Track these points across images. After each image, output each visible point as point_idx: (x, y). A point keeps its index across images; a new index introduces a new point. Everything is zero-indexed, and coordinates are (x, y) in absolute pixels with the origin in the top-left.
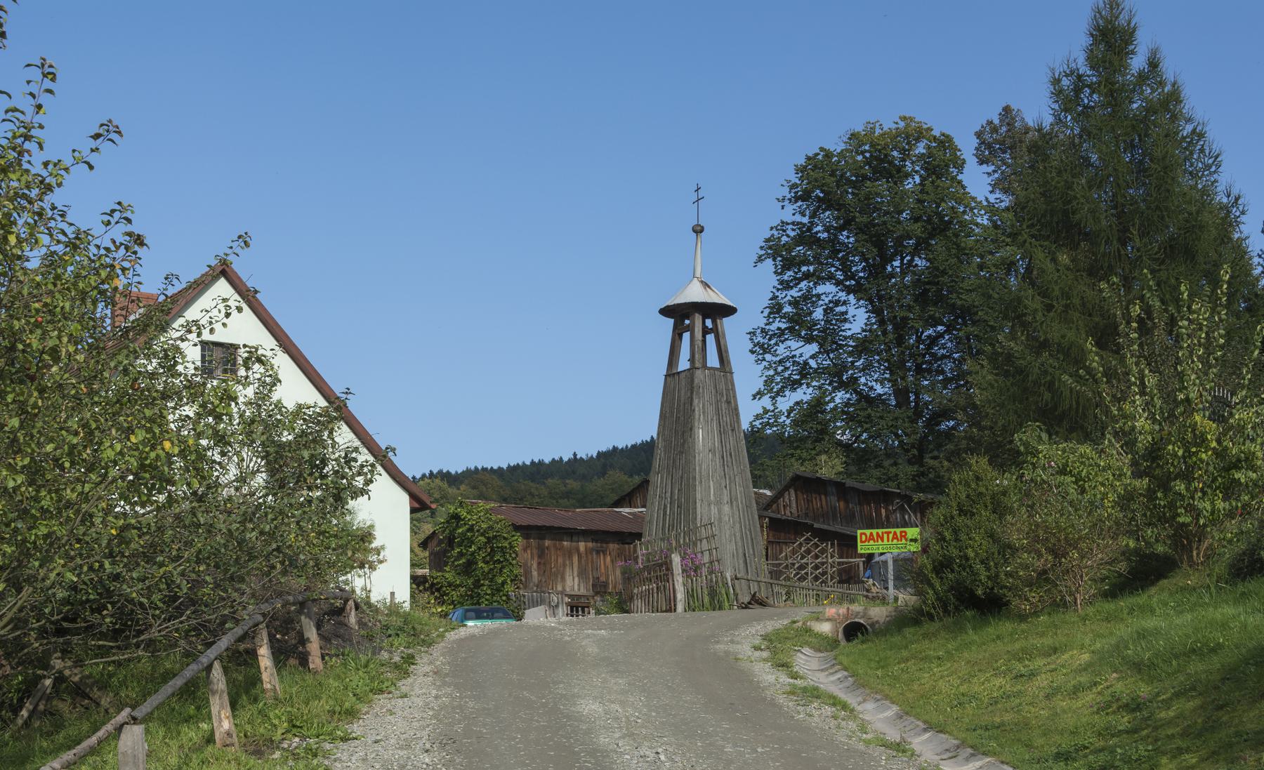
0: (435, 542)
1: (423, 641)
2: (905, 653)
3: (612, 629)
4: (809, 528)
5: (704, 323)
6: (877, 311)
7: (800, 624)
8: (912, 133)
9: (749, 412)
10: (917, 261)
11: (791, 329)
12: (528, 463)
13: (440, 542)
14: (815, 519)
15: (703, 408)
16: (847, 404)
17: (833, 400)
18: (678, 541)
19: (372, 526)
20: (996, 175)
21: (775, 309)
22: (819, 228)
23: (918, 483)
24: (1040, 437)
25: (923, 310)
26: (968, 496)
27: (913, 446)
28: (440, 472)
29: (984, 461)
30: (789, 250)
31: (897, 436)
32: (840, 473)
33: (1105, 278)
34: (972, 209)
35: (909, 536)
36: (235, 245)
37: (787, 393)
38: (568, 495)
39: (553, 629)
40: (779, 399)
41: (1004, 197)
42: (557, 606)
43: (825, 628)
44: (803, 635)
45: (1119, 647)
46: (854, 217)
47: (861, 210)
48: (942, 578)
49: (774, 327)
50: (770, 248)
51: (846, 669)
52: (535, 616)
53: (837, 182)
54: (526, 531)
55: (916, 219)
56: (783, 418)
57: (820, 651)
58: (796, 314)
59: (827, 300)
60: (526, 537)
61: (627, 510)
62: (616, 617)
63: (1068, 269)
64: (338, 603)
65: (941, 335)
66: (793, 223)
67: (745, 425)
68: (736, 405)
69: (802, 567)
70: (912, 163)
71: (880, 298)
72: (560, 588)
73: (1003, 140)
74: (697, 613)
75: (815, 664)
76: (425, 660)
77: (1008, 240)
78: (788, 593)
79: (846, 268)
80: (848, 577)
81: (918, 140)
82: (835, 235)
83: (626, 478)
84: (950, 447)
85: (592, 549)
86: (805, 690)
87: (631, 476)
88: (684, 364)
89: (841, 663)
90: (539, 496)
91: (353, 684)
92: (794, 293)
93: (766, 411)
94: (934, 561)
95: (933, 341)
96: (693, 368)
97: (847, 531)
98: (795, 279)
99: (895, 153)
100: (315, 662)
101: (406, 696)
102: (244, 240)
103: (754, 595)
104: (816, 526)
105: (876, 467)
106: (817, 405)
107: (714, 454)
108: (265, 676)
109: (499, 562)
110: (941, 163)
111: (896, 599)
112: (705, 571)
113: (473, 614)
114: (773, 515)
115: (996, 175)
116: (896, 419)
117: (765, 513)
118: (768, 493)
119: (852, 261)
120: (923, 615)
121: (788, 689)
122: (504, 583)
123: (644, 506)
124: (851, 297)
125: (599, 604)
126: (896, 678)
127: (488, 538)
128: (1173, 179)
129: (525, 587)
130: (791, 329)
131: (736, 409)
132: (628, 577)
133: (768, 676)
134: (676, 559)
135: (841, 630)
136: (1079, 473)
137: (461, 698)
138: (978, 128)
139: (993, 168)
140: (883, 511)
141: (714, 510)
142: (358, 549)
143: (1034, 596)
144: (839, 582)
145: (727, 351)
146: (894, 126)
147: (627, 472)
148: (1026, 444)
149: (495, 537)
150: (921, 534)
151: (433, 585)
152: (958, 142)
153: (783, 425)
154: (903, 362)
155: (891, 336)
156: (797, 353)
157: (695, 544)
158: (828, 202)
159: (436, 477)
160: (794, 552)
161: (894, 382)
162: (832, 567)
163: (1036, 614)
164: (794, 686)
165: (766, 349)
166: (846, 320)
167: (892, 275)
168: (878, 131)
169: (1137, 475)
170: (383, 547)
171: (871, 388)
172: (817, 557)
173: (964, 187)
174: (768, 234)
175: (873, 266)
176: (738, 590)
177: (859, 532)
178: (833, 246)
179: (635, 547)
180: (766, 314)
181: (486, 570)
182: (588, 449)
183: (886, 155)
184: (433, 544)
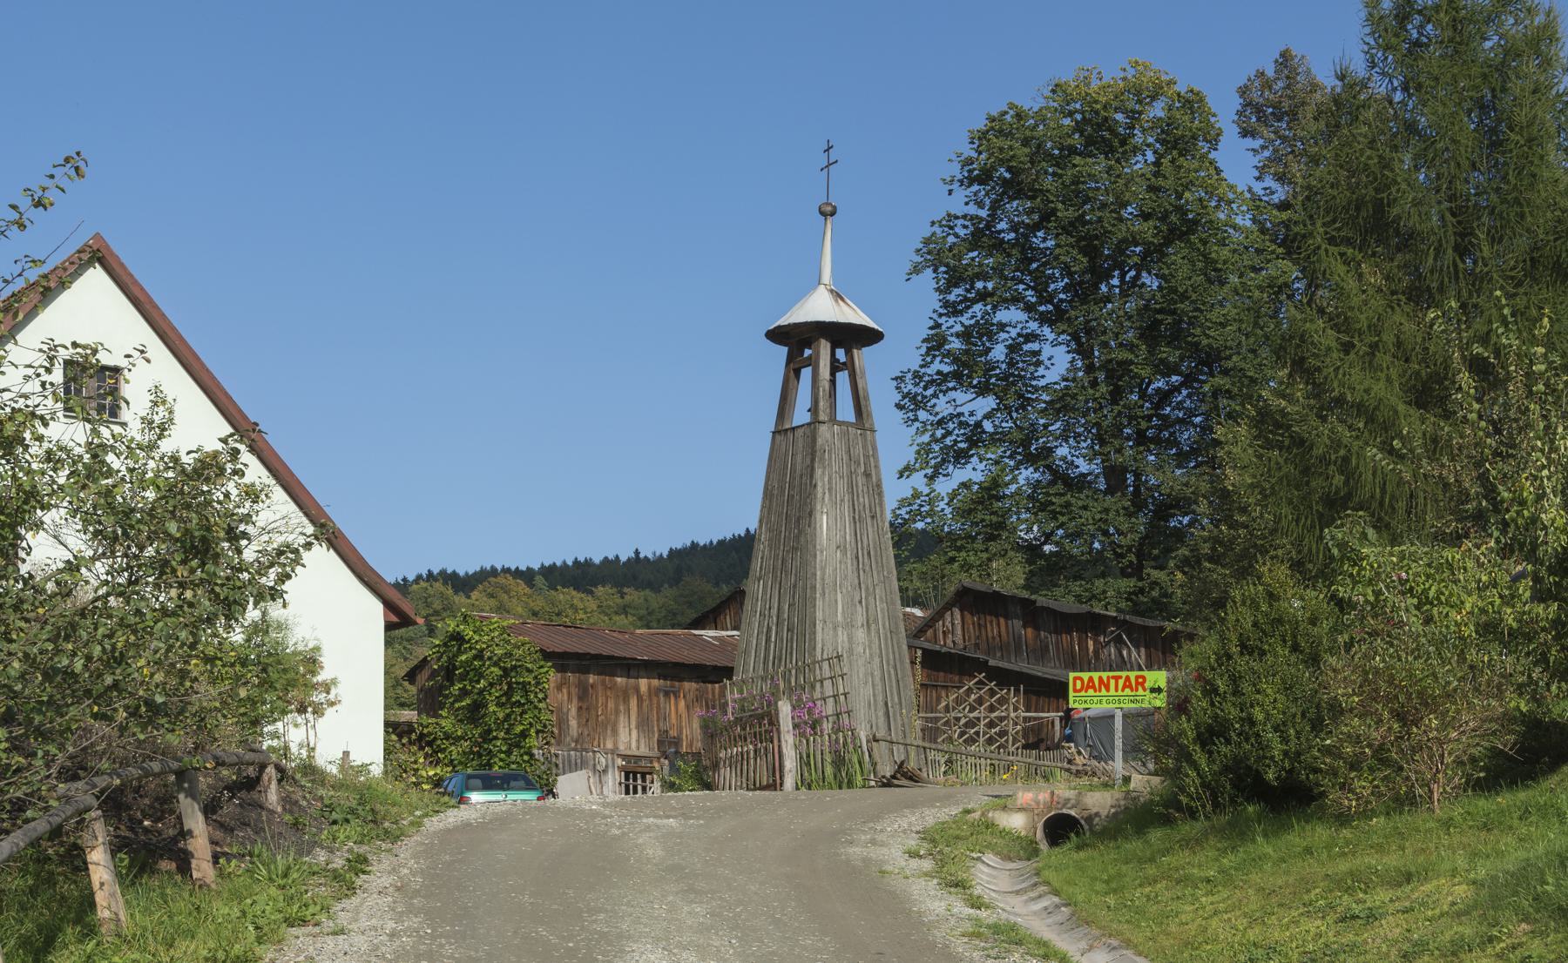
0: (425, 674)
1: (386, 832)
2: (1151, 871)
3: (686, 816)
4: (982, 666)
5: (833, 354)
6: (1083, 351)
7: (977, 815)
8: (1144, 92)
9: (895, 491)
10: (1146, 279)
11: (957, 376)
13: (434, 674)
14: (990, 651)
15: (829, 482)
16: (1037, 485)
19: (317, 649)
20: (1267, 154)
21: (936, 343)
22: (1003, 225)
23: (1135, 604)
24: (1364, 535)
25: (1151, 352)
26: (1255, 624)
27: (1129, 549)
28: (443, 573)
29: (1283, 571)
31: (1106, 533)
33: (1433, 303)
34: (1230, 203)
36: (58, 172)
41: (1274, 185)
42: (605, 771)
43: (1016, 822)
44: (982, 833)
45: (1523, 877)
47: (1062, 210)
48: (1210, 753)
50: (929, 253)
51: (1056, 893)
52: (573, 788)
54: (563, 661)
55: (1146, 217)
57: (1010, 859)
58: (966, 352)
59: (1014, 334)
60: (561, 669)
61: (712, 633)
62: (695, 797)
63: (1380, 290)
64: (251, 771)
65: (1176, 389)
66: (964, 217)
68: (879, 480)
69: (971, 724)
70: (1144, 131)
72: (609, 745)
73: (1274, 106)
74: (816, 793)
75: (1004, 882)
76: (386, 865)
77: (1281, 250)
78: (949, 762)
79: (1040, 287)
80: (1036, 740)
81: (1153, 98)
82: (1026, 236)
84: (1184, 552)
85: (658, 690)
86: (996, 929)
87: (717, 584)
88: (801, 416)
89: (1047, 883)
91: (258, 909)
92: (966, 319)
93: (916, 495)
94: (1197, 726)
95: (1165, 396)
96: (815, 422)
97: (1046, 671)
98: (966, 299)
99: (1119, 117)
100: (203, 868)
101: (342, 932)
102: (74, 165)
104: (992, 663)
106: (991, 491)
107: (844, 553)
108: (100, 898)
110: (1184, 137)
112: (827, 726)
113: (478, 782)
114: (927, 645)
115: (1267, 154)
116: (1107, 511)
117: (917, 643)
118: (918, 612)
121: (968, 927)
124: (1046, 330)
126: (1140, 911)
127: (504, 669)
128: (1542, 157)
129: (559, 743)
130: (957, 376)
131: (879, 486)
132: (711, 733)
133: (934, 902)
134: (785, 709)
135: (1040, 826)
136: (1425, 591)
137: (433, 937)
138: (1243, 81)
139: (1261, 142)
140: (1091, 643)
141: (842, 636)
142: (289, 679)
143: (1362, 785)
144: (1025, 747)
145: (867, 398)
147: (709, 580)
148: (1342, 545)
149: (514, 668)
151: (422, 736)
152: (1212, 103)
154: (1119, 429)
156: (965, 409)
158: (1015, 188)
159: (436, 580)
160: (958, 701)
161: (1106, 458)
163: (1366, 814)
164: (978, 922)
166: (1038, 364)
168: (1095, 84)
169: (1540, 596)
170: (334, 682)
172: (992, 709)
173: (1218, 171)
175: (1081, 283)
177: (1072, 675)
180: (923, 350)
181: (501, 715)
182: (656, 546)
184: (422, 678)
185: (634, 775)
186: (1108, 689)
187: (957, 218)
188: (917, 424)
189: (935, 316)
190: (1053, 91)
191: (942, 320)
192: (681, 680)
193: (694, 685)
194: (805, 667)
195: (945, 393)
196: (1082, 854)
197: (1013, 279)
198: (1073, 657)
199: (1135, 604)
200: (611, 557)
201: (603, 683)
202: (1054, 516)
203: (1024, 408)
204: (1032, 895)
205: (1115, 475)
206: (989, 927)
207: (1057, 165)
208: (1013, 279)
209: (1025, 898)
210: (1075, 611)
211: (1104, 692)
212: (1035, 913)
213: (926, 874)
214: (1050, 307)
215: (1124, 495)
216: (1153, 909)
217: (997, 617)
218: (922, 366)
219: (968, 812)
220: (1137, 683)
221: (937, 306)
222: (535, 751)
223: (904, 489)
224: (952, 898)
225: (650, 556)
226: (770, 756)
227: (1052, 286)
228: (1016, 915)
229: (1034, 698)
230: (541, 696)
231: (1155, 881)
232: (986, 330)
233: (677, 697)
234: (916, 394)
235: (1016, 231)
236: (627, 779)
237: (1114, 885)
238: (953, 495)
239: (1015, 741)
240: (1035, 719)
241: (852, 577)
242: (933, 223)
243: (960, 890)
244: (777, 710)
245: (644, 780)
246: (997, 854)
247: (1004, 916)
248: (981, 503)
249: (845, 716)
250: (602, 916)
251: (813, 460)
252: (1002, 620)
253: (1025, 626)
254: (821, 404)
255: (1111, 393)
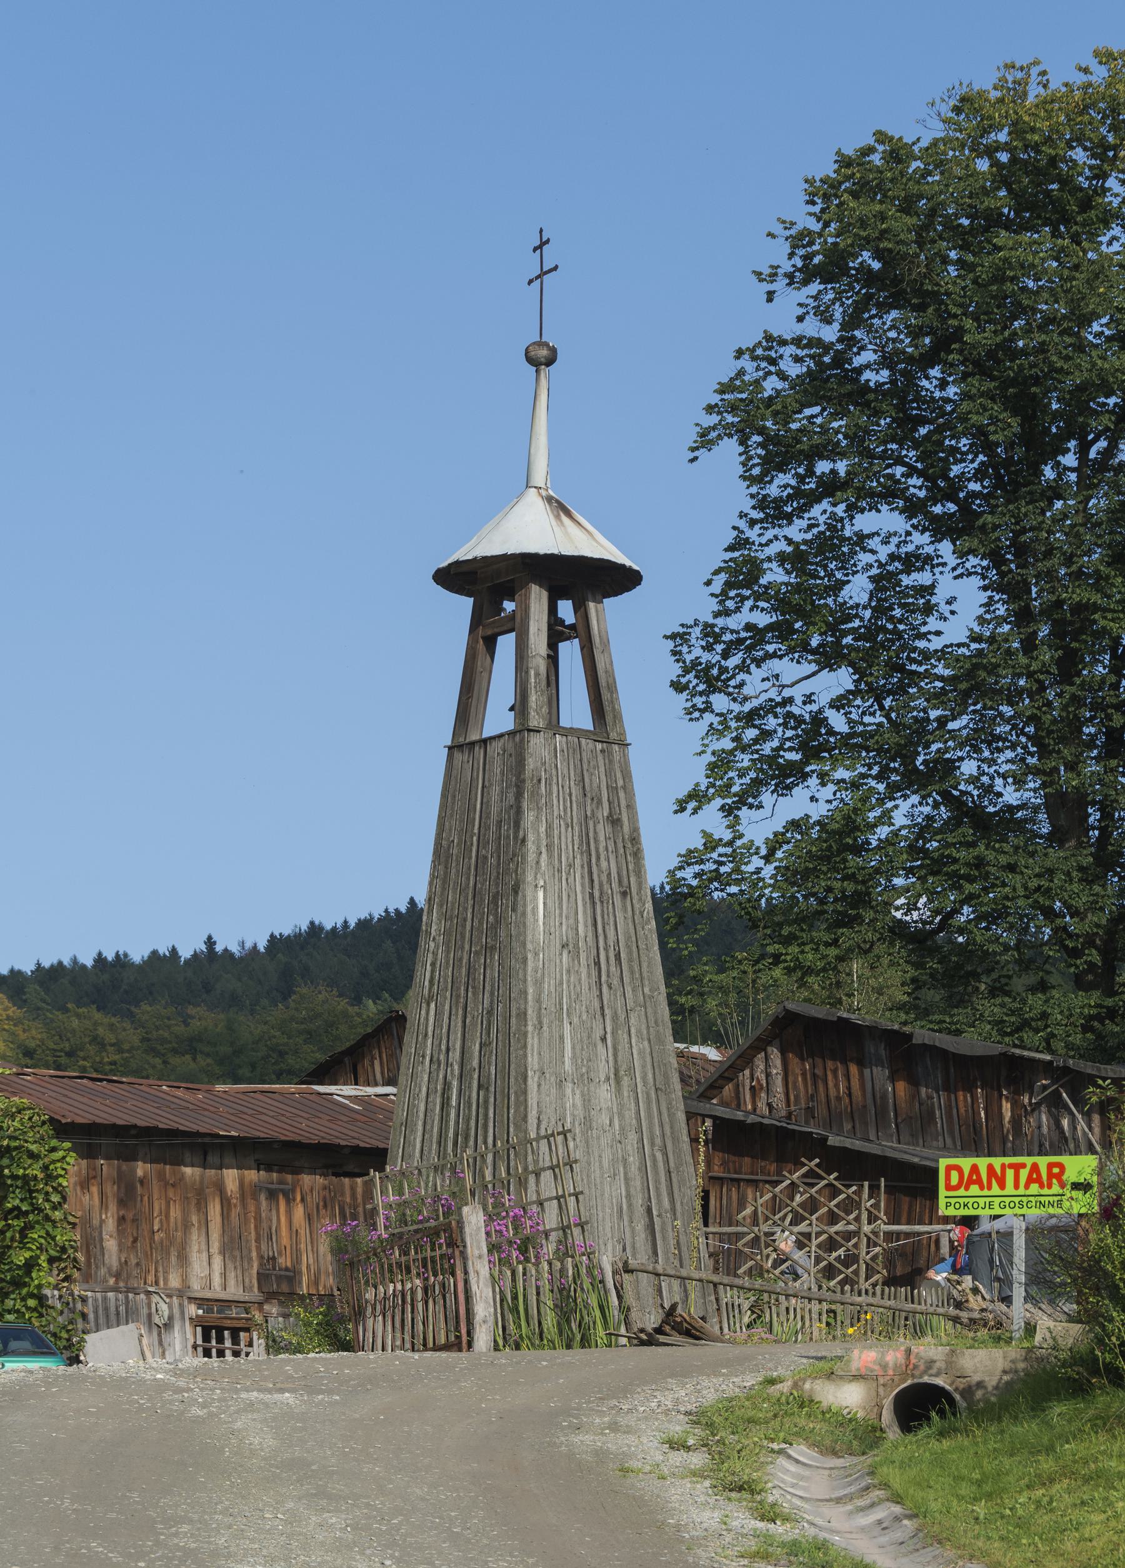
2: (1047, 1464)
3: (312, 1390)
4: (816, 1146)
5: (553, 610)
6: (1009, 587)
7: (785, 1387)
9: (666, 843)
11: (782, 630)
12: (88, 961)
14: (833, 1120)
16: (924, 829)
17: (886, 818)
18: (478, 1173)
21: (741, 575)
22: (868, 357)
27: (1090, 941)
30: (784, 416)
31: (1050, 914)
32: (901, 1007)
35: (1071, 1176)
37: (767, 798)
38: (191, 1045)
39: (161, 1387)
40: (744, 813)
42: (169, 1325)
43: (849, 1397)
44: (792, 1414)
46: (960, 331)
49: (735, 622)
50: (733, 408)
51: (897, 1499)
52: (110, 1350)
53: (921, 230)
54: (89, 1138)
56: (757, 862)
57: (835, 1453)
58: (798, 588)
59: (883, 553)
60: (88, 1152)
61: (349, 1090)
62: (323, 1361)
66: (797, 341)
67: (656, 874)
68: (635, 830)
71: (1021, 551)
72: (174, 1282)
74: (526, 1354)
75: (820, 1485)
79: (934, 469)
83: (343, 1004)
85: (256, 1189)
88: (497, 718)
89: (885, 1485)
90: (118, 1046)
93: (711, 844)
96: (522, 730)
98: (798, 493)
99: (1079, 155)
103: (671, 1312)
104: (833, 1140)
105: (993, 992)
106: (841, 837)
107: (575, 954)
109: (17, 1212)
111: (1030, 1329)
112: (549, 1248)
116: (1051, 872)
117: (704, 1107)
118: (712, 1053)
119: (954, 450)
120: (1096, 1372)
121: (753, 1545)
122: (30, 1265)
123: (391, 1081)
125: (276, 1323)
126: (1022, 1524)
129: (87, 1278)
130: (782, 630)
131: (635, 839)
132: (350, 1260)
133: (701, 1511)
134: (474, 1219)
135: (888, 1403)
140: (1006, 1107)
141: (573, 1097)
144: (887, 1282)
145: (612, 688)
146: (1080, 79)
147: (342, 991)
150: (1101, 1170)
153: (756, 879)
154: (1076, 726)
155: (1046, 655)
156: (798, 693)
157: (522, 1183)
158: (892, 286)
161: (1048, 776)
162: (871, 1243)
165: (715, 681)
166: (928, 609)
167: (1056, 491)
171: (988, 789)
172: (833, 1218)
174: (727, 370)
175: (1008, 462)
176: (630, 1298)
178: (902, 407)
179: (369, 1187)
180: (717, 587)
182: (244, 929)
183: (1053, 161)
185: (219, 1331)
186: (1002, 1186)
187: (783, 343)
188: (709, 718)
189: (742, 524)
190: (957, 110)
191: (752, 534)
192: (296, 1171)
193: (320, 1180)
194: (511, 1149)
195: (759, 662)
196: (946, 1443)
197: (883, 456)
198: (976, 1130)
199: (1100, 1036)
200: (163, 950)
201: (161, 1177)
202: (956, 881)
203: (900, 690)
204: (861, 1503)
205: (1066, 807)
206: (783, 1545)
207: (965, 247)
208: (883, 456)
209: (849, 1507)
210: (979, 1052)
211: (996, 1189)
212: (863, 1529)
213: (694, 1474)
214: (952, 507)
215: (1080, 845)
216: (1044, 1519)
217: (844, 1062)
218: (717, 615)
219: (772, 1382)
220: (1050, 1175)
221: (747, 504)
222: (47, 1292)
223: (689, 832)
224: (731, 1506)
225: (235, 949)
226: (450, 1298)
227: (956, 470)
228: (833, 1531)
229: (905, 1200)
230: (55, 1198)
231: (1052, 1481)
232: (832, 546)
233: (289, 1201)
234: (709, 666)
235: (891, 368)
236: (206, 1338)
237: (987, 1488)
238: (775, 843)
239: (870, 1272)
240: (908, 1235)
241: (589, 997)
242: (739, 353)
243: (745, 1495)
244: (460, 1224)
245: (235, 1340)
246: (813, 1445)
247: (811, 1531)
248: (828, 859)
249: (576, 1231)
250: (185, 1528)
251: (519, 795)
252: (854, 1069)
253: (893, 1079)
254: (533, 698)
255: (1059, 662)
